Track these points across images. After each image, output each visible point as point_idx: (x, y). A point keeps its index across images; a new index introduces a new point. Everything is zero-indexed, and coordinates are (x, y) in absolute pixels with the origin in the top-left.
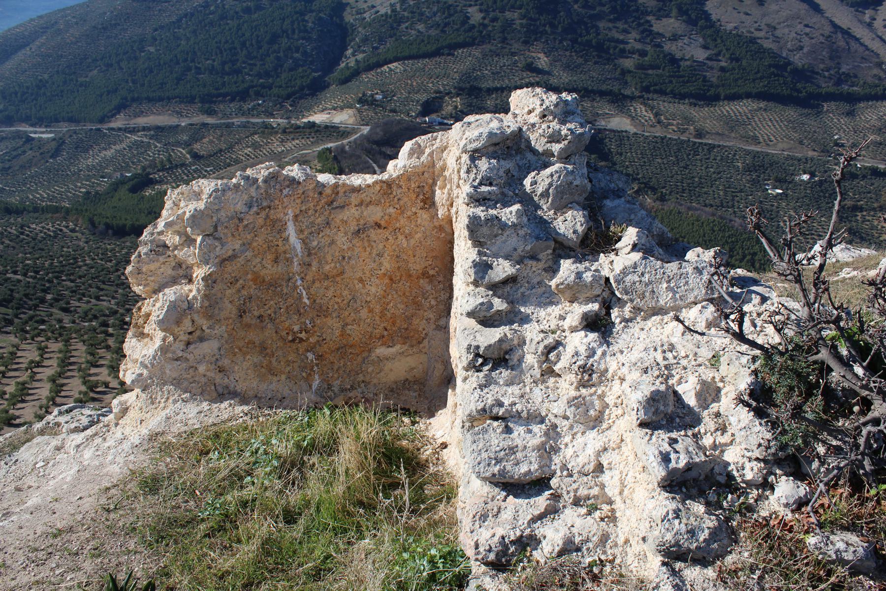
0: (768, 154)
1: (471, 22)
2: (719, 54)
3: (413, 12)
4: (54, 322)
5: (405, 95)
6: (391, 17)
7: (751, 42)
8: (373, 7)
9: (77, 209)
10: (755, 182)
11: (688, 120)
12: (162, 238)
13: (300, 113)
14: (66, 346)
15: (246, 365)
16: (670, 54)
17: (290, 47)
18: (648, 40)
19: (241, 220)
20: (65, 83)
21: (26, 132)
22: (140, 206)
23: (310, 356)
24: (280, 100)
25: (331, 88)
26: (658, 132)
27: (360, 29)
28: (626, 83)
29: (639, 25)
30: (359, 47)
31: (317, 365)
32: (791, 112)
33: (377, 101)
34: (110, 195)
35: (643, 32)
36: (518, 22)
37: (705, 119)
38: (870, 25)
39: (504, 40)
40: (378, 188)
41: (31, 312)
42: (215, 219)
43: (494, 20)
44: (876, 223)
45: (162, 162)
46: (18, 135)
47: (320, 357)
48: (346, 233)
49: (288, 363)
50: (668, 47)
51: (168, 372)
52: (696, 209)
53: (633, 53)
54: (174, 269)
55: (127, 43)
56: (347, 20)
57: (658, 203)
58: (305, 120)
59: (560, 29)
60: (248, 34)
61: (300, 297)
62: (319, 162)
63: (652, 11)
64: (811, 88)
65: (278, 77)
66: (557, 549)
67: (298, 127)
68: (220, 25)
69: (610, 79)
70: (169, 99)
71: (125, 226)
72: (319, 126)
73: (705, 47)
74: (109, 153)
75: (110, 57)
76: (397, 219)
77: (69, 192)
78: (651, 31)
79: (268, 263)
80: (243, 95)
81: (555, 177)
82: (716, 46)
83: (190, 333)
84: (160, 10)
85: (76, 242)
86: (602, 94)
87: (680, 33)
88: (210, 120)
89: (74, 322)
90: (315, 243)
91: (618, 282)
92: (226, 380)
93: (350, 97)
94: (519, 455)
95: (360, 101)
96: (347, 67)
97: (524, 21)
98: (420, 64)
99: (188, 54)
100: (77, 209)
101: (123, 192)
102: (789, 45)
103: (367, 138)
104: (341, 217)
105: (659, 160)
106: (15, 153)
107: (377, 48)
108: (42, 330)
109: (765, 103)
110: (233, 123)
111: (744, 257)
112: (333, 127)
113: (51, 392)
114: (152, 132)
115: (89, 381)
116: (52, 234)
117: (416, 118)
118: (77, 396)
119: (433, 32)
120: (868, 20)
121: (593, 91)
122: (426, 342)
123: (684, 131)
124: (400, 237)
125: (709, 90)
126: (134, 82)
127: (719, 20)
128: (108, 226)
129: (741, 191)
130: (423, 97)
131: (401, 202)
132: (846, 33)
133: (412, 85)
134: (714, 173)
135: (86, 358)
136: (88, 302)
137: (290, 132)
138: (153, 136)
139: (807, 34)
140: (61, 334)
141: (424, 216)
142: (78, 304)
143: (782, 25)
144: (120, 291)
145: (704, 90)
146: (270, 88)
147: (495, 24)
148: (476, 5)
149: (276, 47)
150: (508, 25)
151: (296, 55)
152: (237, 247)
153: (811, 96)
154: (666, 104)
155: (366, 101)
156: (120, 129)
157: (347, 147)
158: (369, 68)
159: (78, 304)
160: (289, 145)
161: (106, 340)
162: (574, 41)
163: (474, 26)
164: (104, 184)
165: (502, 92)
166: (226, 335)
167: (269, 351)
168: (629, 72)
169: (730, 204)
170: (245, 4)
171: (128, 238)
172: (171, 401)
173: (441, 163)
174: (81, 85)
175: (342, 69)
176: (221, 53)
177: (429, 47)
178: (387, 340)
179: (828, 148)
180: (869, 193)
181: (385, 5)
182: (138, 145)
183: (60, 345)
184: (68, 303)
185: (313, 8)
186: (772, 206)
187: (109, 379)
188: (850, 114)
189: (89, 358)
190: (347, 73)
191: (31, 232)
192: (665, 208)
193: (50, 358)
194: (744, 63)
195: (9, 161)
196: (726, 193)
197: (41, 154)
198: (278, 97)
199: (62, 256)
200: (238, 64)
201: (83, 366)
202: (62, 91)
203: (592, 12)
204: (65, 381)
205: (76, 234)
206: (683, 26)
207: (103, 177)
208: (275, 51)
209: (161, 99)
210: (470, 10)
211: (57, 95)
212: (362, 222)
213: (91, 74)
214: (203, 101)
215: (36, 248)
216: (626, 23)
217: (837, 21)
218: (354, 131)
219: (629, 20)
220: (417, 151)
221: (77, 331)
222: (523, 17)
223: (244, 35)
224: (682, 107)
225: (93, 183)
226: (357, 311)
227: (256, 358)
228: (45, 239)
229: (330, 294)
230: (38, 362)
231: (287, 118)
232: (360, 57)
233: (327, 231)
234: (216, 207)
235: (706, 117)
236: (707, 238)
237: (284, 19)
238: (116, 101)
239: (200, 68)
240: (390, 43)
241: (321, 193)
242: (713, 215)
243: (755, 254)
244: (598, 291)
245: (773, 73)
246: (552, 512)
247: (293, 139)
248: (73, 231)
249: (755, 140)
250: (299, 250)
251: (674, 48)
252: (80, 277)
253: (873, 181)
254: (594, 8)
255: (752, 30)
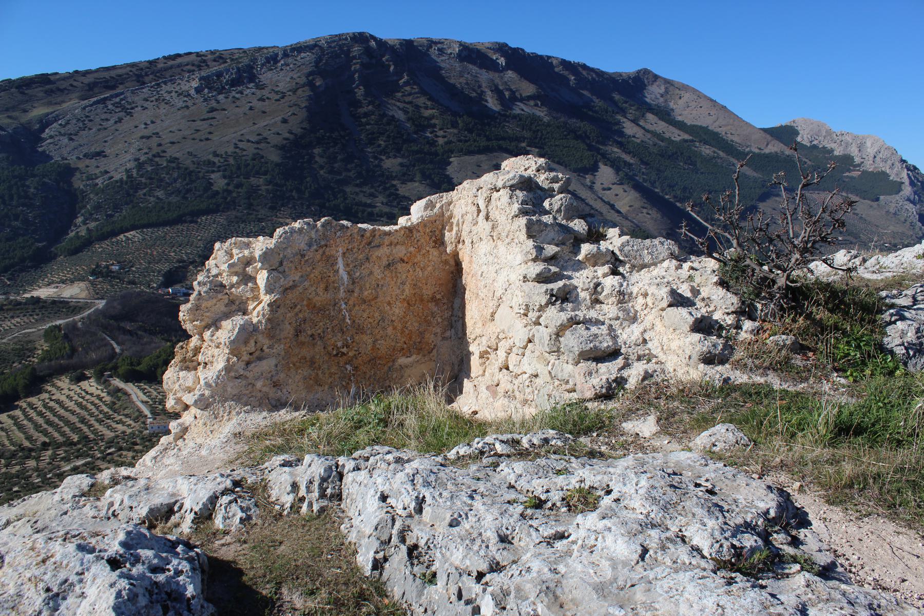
1: (215, 188)
3: (151, 179)
5: (144, 265)
6: (126, 183)
8: (106, 172)
12: (220, 279)
15: (298, 377)
19: (303, 256)
23: (349, 367)
27: (92, 196)
29: (385, 189)
30: (91, 214)
31: (354, 375)
33: (113, 272)
35: (389, 196)
36: (263, 188)
39: (250, 206)
40: (403, 232)
42: (281, 256)
43: (239, 186)
47: (356, 368)
48: (379, 267)
49: (331, 375)
51: (229, 389)
54: (226, 305)
56: (76, 186)
58: (27, 295)
59: (307, 194)
61: (344, 318)
62: (46, 341)
63: (396, 176)
66: (641, 378)
67: (20, 303)
72: (45, 302)
76: (415, 256)
78: (397, 195)
79: (320, 291)
81: (564, 200)
83: (251, 354)
90: (358, 274)
91: (621, 250)
92: (280, 393)
93: (82, 269)
94: (600, 338)
95: (93, 273)
96: (77, 236)
97: (270, 187)
98: (160, 232)
104: (376, 254)
107: (111, 216)
117: (157, 289)
119: (174, 199)
122: (435, 351)
124: (418, 269)
130: (165, 267)
131: (419, 243)
133: (152, 255)
137: (10, 310)
141: (435, 253)
147: (240, 190)
148: (219, 171)
150: (253, 191)
152: (297, 278)
155: (101, 272)
158: (103, 237)
163: (217, 193)
166: (283, 353)
167: (317, 365)
172: (234, 413)
173: (449, 213)
175: (71, 239)
178: (407, 353)
181: (120, 170)
203: (338, 177)
210: (213, 176)
212: (391, 258)
216: (372, 187)
218: (87, 306)
220: (430, 206)
222: (269, 183)
226: (384, 328)
227: (306, 371)
229: (365, 315)
232: (92, 225)
233: (367, 265)
234: (284, 246)
240: (126, 211)
241: (363, 236)
244: (608, 258)
246: (627, 365)
247: (12, 317)
250: (346, 279)
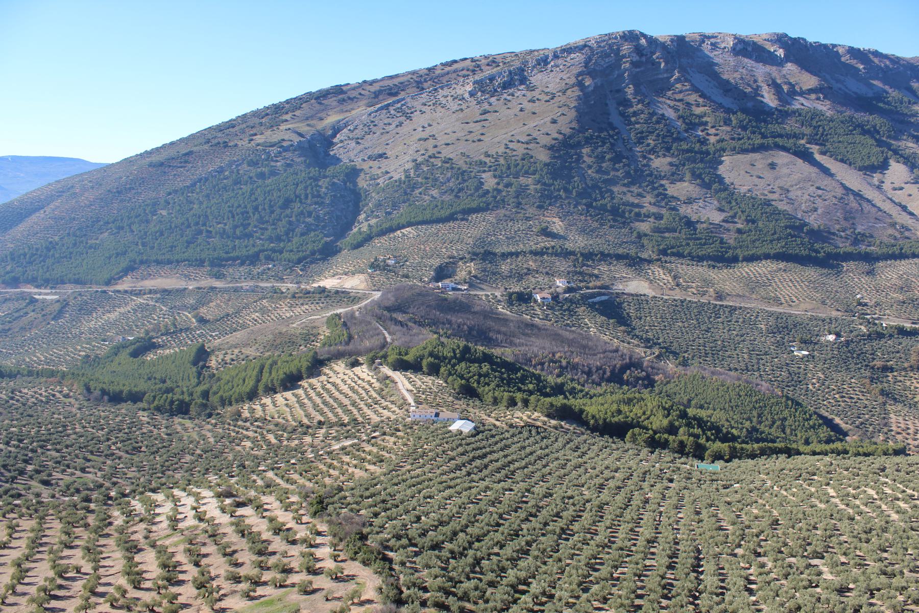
0: (790, 315)
1: (485, 187)
2: (734, 216)
3: (427, 178)
4: (31, 497)
5: (418, 260)
6: (404, 182)
7: (765, 204)
8: (387, 173)
9: (73, 374)
10: (779, 344)
11: (707, 282)
13: (311, 278)
14: (40, 524)
16: (686, 217)
17: (302, 211)
18: (663, 204)
20: (75, 244)
21: (30, 293)
22: (140, 371)
24: (291, 264)
25: (343, 252)
26: (678, 295)
27: (373, 194)
28: (643, 246)
29: (654, 189)
30: (373, 212)
32: (811, 273)
34: (110, 359)
35: (657, 196)
36: (532, 187)
37: (724, 281)
38: (879, 188)
41: (8, 485)
43: (508, 185)
44: (908, 383)
45: (166, 326)
46: (22, 296)
50: (685, 210)
52: (721, 374)
53: (649, 217)
55: (140, 206)
57: (680, 367)
58: (315, 285)
60: (260, 199)
64: (829, 248)
65: (289, 241)
68: (233, 190)
69: (626, 243)
70: (178, 262)
71: (121, 392)
73: (721, 210)
74: (113, 316)
75: (122, 219)
77: (67, 355)
80: (253, 259)
82: (731, 208)
84: (175, 175)
85: (69, 408)
86: (619, 257)
87: (694, 196)
88: (218, 284)
89: (53, 496)
95: (372, 266)
97: (539, 187)
98: (434, 228)
99: (199, 217)
100: (73, 374)
101: (124, 356)
102: (803, 207)
103: (378, 304)
105: (680, 324)
106: (16, 315)
107: (390, 213)
108: (16, 505)
109: (784, 263)
110: (242, 287)
111: (774, 423)
112: (343, 292)
113: (13, 578)
114: (158, 296)
115: (59, 565)
116: (44, 399)
118: (42, 583)
119: (447, 198)
120: (877, 183)
121: (609, 255)
123: (704, 294)
125: (726, 252)
126: (144, 245)
127: (732, 184)
128: (104, 392)
129: (766, 354)
130: (436, 262)
132: (858, 195)
134: (737, 335)
135: (60, 538)
136: (73, 474)
138: (159, 299)
139: (820, 196)
140: (38, 510)
142: (61, 476)
143: (795, 187)
144: (109, 462)
145: (722, 252)
146: (281, 252)
149: (288, 211)
150: (521, 192)
151: (308, 220)
153: (829, 256)
154: (684, 267)
156: (126, 292)
157: (357, 313)
158: (382, 233)
159: (61, 476)
160: (298, 310)
161: (86, 517)
162: (589, 206)
163: (488, 192)
164: (104, 349)
165: (517, 256)
168: (646, 235)
169: (755, 367)
170: (259, 170)
171: (124, 405)
174: (91, 247)
176: (233, 217)
177: (442, 212)
179: (852, 307)
180: (898, 352)
181: (399, 171)
182: (143, 308)
183: (33, 523)
184: (50, 475)
185: (327, 173)
186: (799, 368)
187: (82, 563)
188: (870, 273)
189: (64, 538)
190: (360, 238)
191: (22, 397)
192: (688, 373)
193: (20, 538)
194: (760, 224)
195: (10, 322)
196: (750, 358)
197: (44, 315)
198: (289, 261)
199: (51, 423)
200: (250, 229)
201: (55, 547)
202: (71, 253)
204: (32, 565)
205: (69, 400)
206: (698, 189)
207: (104, 340)
208: (287, 216)
209: (170, 262)
210: (484, 175)
211: (66, 257)
213: (102, 236)
214: (212, 264)
215: (25, 414)
216: (640, 187)
217: (848, 184)
218: (365, 296)
219: (644, 184)
221: (55, 507)
223: (256, 199)
224: (701, 269)
225: (94, 346)
228: (35, 404)
230: (5, 543)
231: (297, 283)
232: (373, 221)
235: (725, 279)
236: (733, 404)
237: (297, 185)
238: (124, 263)
239: (211, 232)
240: (403, 208)
242: (739, 379)
243: (785, 419)
245: (790, 234)
247: (302, 304)
248: (67, 396)
249: (777, 301)
251: (689, 211)
252: (67, 447)
253: (901, 340)
254: (607, 173)
255: (766, 192)
